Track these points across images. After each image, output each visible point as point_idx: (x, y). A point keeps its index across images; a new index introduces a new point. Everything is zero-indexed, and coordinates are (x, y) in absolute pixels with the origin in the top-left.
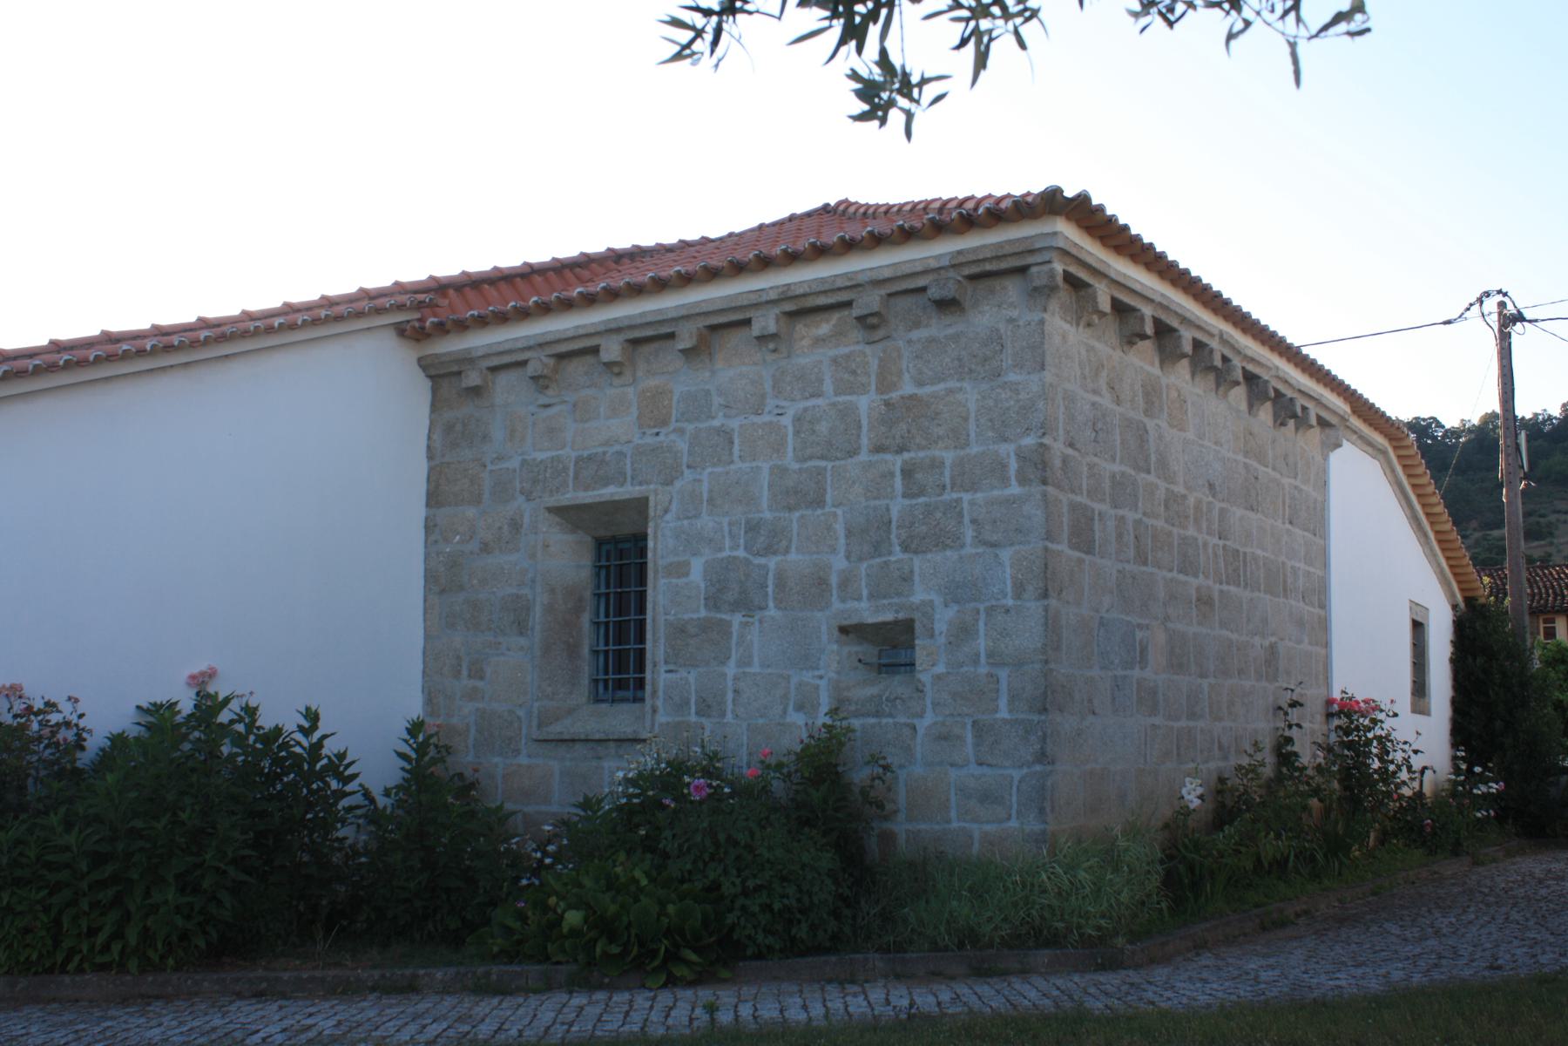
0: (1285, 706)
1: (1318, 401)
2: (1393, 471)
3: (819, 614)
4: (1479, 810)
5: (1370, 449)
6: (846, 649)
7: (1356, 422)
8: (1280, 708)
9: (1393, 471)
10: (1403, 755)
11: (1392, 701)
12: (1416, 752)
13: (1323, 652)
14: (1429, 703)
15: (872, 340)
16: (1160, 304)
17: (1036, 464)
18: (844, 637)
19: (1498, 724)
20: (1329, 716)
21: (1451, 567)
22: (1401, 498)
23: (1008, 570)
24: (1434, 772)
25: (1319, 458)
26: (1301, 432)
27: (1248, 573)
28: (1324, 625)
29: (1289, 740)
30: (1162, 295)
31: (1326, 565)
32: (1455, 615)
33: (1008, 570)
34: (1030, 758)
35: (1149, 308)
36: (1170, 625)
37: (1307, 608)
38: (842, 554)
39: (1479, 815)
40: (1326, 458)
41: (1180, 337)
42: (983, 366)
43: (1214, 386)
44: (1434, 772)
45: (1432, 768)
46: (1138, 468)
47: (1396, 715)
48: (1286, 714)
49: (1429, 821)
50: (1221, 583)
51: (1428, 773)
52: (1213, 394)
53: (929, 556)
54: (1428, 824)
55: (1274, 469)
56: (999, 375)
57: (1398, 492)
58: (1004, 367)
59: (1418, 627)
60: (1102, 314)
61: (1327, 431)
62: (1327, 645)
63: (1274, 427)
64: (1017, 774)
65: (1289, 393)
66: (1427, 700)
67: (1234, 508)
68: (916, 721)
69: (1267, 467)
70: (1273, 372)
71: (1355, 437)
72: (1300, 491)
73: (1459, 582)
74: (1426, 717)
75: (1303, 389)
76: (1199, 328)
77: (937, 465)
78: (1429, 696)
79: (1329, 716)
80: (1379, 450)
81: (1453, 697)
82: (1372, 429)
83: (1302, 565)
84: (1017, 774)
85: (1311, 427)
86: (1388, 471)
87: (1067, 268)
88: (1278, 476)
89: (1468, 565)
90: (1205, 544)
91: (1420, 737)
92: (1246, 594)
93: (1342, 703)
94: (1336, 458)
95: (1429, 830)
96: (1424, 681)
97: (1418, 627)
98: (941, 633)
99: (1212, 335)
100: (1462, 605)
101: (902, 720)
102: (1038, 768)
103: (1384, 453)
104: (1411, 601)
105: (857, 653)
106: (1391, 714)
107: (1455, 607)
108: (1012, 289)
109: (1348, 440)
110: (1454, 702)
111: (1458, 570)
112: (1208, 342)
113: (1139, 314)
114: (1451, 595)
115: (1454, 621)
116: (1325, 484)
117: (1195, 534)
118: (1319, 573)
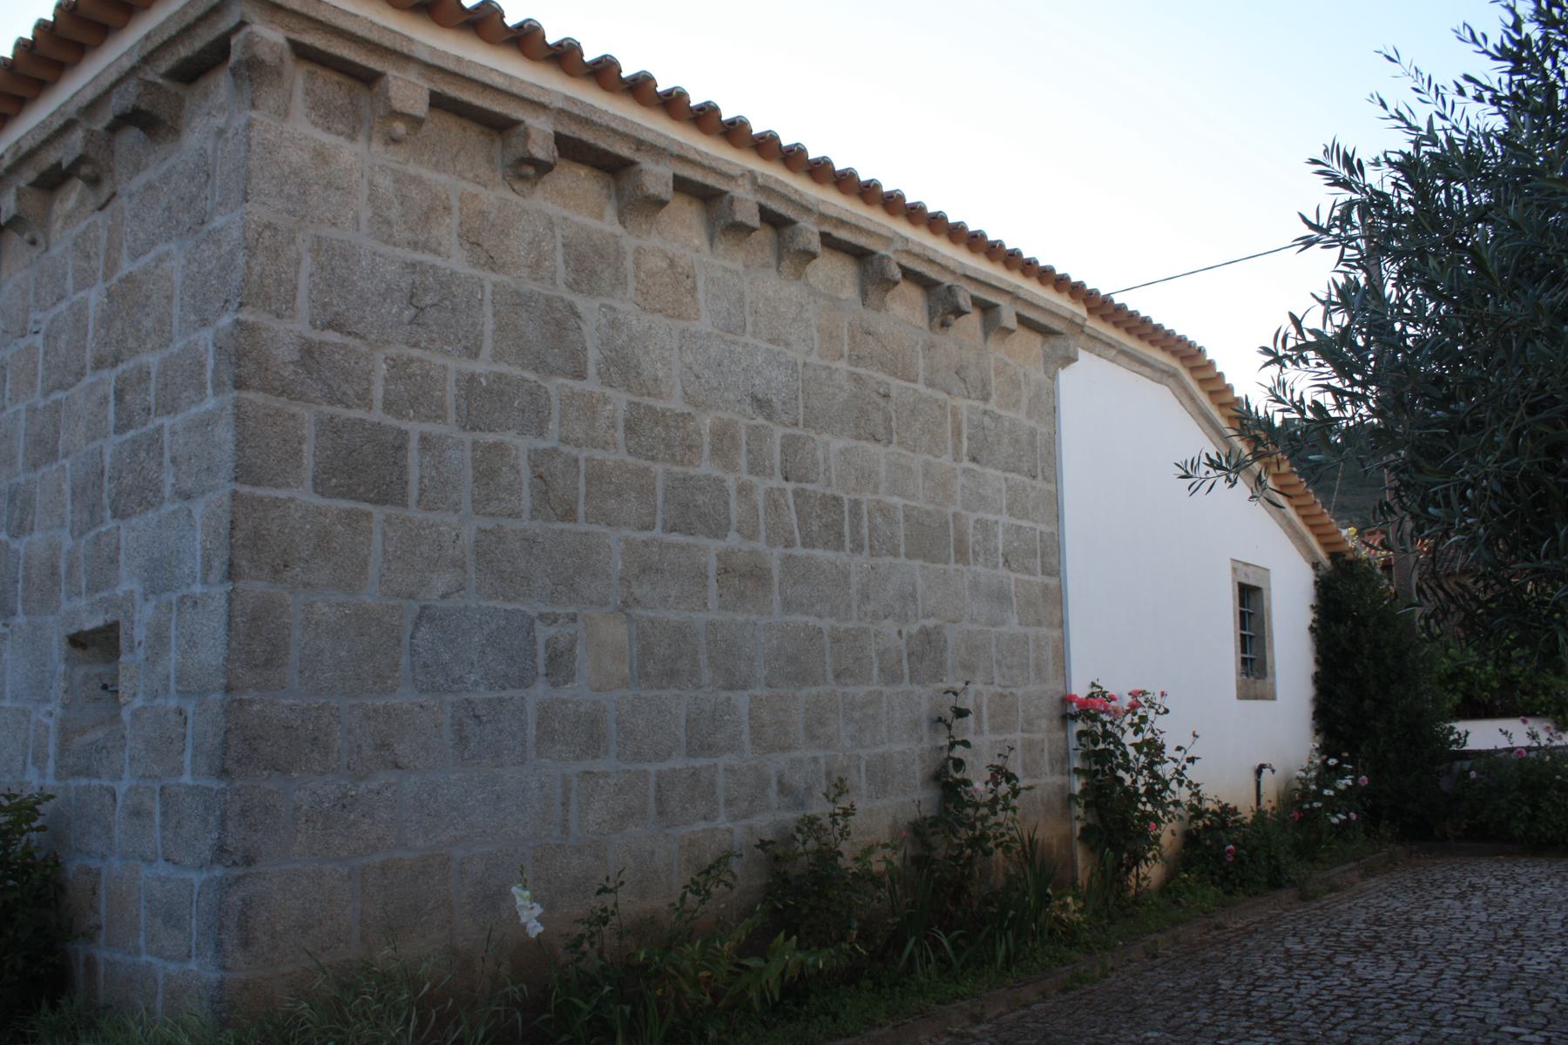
0: (949, 715)
1: (1014, 296)
2: (1193, 399)
3: (51, 619)
4: (1334, 814)
5: (1147, 371)
6: (81, 671)
7: (1095, 325)
8: (940, 720)
9: (1193, 399)
10: (1175, 765)
11: (1163, 694)
12: (1191, 760)
13: (1056, 633)
14: (1273, 684)
15: (103, 200)
16: (561, 111)
17: (230, 355)
18: (78, 653)
19: (1368, 704)
20: (1066, 718)
21: (1304, 517)
22: (1209, 430)
23: (199, 536)
24: (1273, 771)
25: (1040, 375)
26: (992, 338)
27: (865, 531)
28: (1056, 598)
29: (959, 764)
30: (567, 98)
31: (1058, 517)
32: (1317, 576)
33: (199, 536)
34: (207, 854)
35: (543, 119)
36: (638, 611)
37: (1013, 576)
38: (68, 529)
39: (1335, 820)
40: (1054, 378)
41: (732, 200)
42: (189, 211)
43: (773, 261)
44: (1273, 771)
45: (1270, 767)
46: (541, 366)
47: (1167, 711)
48: (949, 727)
49: (1231, 847)
50: (789, 544)
51: (1266, 772)
52: (773, 271)
53: (134, 521)
54: (1229, 851)
55: (930, 384)
56: (203, 222)
57: (1206, 426)
58: (208, 208)
59: (1250, 597)
60: (415, 122)
61: (1052, 340)
62: (1062, 624)
63: (931, 327)
64: (197, 878)
65: (947, 280)
66: (1268, 680)
67: (826, 437)
68: (115, 785)
69: (915, 381)
70: (899, 245)
71: (1113, 352)
72: (997, 418)
73: (1318, 536)
74: (1272, 702)
75: (969, 273)
76: (682, 159)
77: (143, 376)
78: (1273, 674)
79: (1066, 718)
80: (1163, 371)
81: (1316, 673)
82: (1146, 344)
83: (1004, 518)
84: (197, 878)
85: (1010, 331)
86: (1187, 403)
87: (294, 36)
88: (942, 396)
89: (1323, 514)
90: (745, 490)
91: (1198, 740)
92: (858, 564)
93: (1083, 704)
94: (1066, 377)
95: (1230, 859)
96: (1265, 657)
97: (1250, 597)
98: (140, 643)
99: (731, 178)
100: (1327, 563)
101: (106, 783)
102: (218, 871)
103: (1173, 375)
104: (1232, 560)
105: (99, 676)
106: (1161, 710)
107: (1315, 566)
108: (221, 85)
109: (1083, 349)
110: (1318, 680)
111: (1314, 521)
112: (724, 187)
113: (522, 128)
114: (1308, 552)
115: (1316, 583)
116: (1055, 410)
117: (717, 473)
118: (1046, 529)
